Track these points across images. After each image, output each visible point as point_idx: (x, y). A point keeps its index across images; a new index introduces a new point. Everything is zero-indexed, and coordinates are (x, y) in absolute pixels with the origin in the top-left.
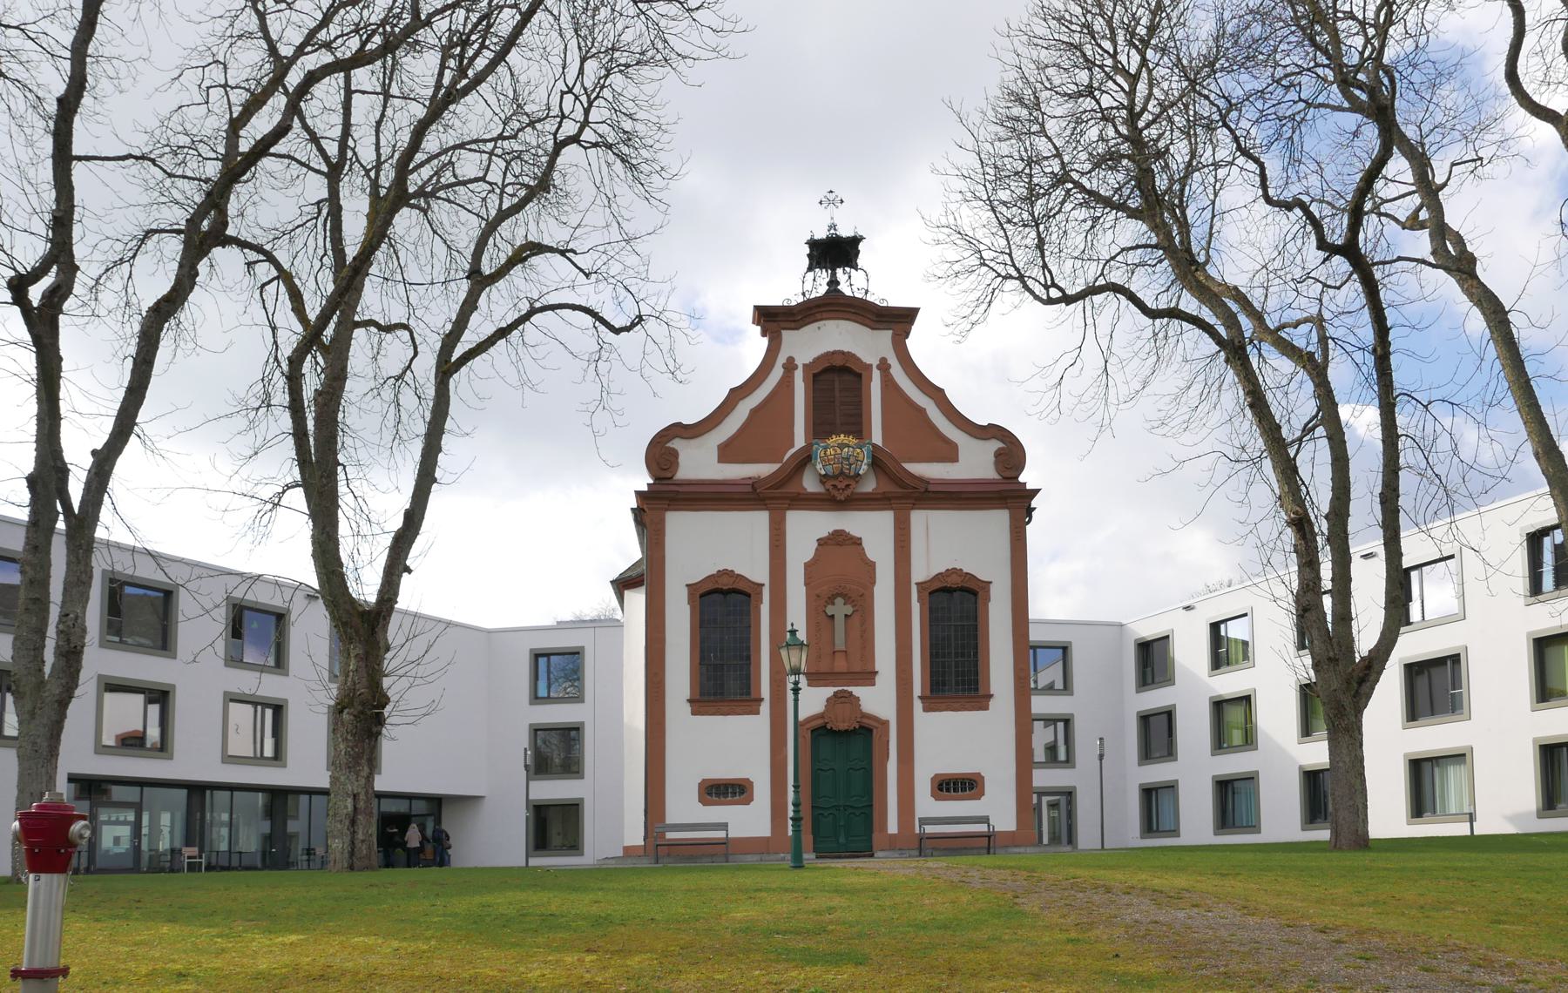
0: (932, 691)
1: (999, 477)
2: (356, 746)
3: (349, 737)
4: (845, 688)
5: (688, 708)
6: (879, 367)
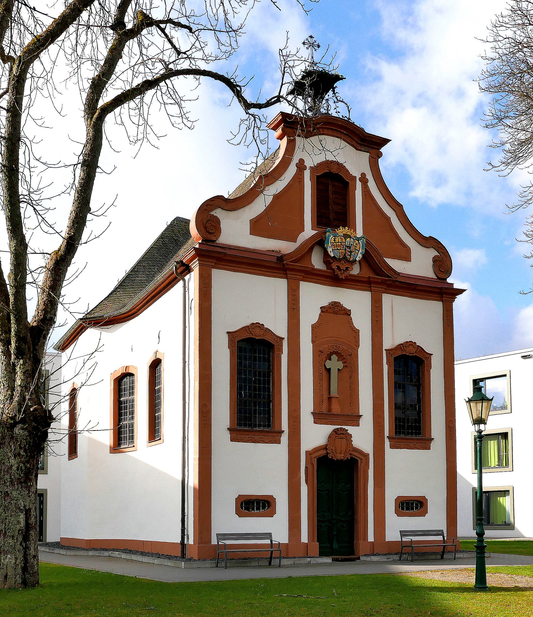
0: (396, 433)
1: (434, 277)
2: (28, 462)
3: (22, 453)
4: (344, 427)
5: (228, 435)
6: (360, 180)
